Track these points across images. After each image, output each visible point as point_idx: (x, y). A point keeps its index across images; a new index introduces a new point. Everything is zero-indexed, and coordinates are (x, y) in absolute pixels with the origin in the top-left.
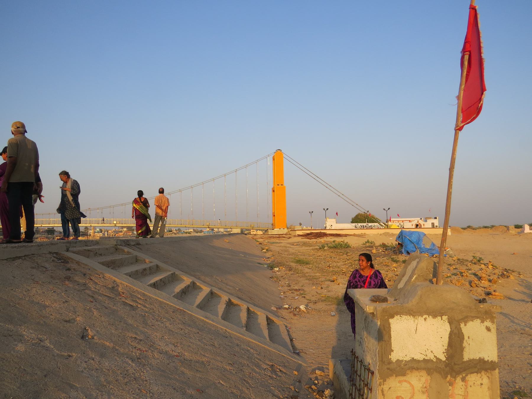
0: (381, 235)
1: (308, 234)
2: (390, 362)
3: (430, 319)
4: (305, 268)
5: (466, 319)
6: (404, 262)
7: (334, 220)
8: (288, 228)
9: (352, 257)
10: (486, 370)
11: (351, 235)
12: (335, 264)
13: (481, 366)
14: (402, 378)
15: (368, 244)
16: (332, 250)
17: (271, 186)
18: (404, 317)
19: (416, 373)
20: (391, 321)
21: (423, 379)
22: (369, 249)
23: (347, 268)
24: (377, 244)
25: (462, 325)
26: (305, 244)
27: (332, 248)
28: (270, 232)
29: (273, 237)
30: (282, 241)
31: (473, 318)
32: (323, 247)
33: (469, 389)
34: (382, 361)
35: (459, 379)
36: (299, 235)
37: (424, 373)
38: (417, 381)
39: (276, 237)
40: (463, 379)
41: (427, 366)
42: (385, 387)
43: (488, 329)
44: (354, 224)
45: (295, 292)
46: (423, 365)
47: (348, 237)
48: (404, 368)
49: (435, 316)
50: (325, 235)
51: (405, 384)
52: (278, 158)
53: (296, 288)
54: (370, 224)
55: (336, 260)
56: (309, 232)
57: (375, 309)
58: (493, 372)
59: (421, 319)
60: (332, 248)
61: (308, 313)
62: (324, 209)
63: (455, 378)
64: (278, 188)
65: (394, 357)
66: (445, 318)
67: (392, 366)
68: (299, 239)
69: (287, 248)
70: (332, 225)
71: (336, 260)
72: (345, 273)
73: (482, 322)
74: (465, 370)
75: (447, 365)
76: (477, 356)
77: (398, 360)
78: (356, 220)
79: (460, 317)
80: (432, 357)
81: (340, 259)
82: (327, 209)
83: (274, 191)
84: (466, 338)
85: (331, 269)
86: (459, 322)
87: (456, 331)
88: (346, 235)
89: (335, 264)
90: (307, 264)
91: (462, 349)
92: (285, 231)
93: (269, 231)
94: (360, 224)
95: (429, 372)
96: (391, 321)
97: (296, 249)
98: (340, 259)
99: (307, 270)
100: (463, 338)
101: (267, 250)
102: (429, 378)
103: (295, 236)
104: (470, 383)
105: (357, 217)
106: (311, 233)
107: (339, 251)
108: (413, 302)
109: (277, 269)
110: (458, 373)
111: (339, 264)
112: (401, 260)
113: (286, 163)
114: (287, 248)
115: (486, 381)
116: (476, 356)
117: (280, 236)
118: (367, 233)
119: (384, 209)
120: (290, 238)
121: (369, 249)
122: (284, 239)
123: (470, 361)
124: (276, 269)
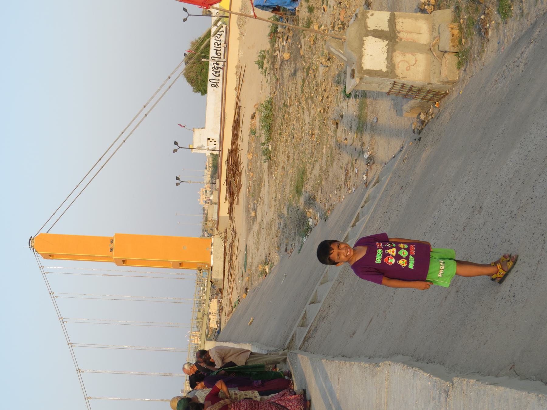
0: (242, 34)
1: (230, 190)
2: (387, 72)
3: (365, 47)
4: (313, 176)
5: (366, 27)
6: (311, 10)
7: (197, 132)
8: (211, 236)
9: (296, 95)
10: (394, 19)
11: (238, 97)
12: (307, 127)
13: (392, 22)
14: (396, 67)
15: (266, 65)
16: (276, 136)
17: (112, 266)
18: (363, 61)
19: (394, 58)
20: (364, 69)
21: (398, 55)
22: (277, 66)
23: (315, 105)
24: (267, 46)
25: (369, 29)
26: (255, 195)
27: (270, 134)
28: (218, 275)
29: (229, 271)
30: (242, 248)
31: (366, 23)
32: (267, 152)
33: (404, 30)
34: (386, 76)
35: (399, 35)
36: (230, 211)
37: (394, 54)
38: (398, 58)
39: (231, 263)
40: (399, 32)
41: (391, 51)
42: (401, 76)
43: (372, 15)
44: (210, 89)
45: (349, 176)
46: (390, 54)
47: (242, 104)
48: (391, 65)
49: (363, 44)
50: (233, 153)
51: (399, 65)
52: (48, 247)
53: (343, 177)
54: (212, 53)
55: (298, 125)
56: (224, 188)
57: (358, 77)
58: (396, 15)
59: (365, 52)
60: (270, 134)
61: (373, 149)
62: (175, 151)
63: (398, 37)
64: (116, 251)
65: (384, 69)
66: (364, 38)
67: (390, 71)
68: (240, 209)
69: (264, 226)
70: (208, 136)
71: (298, 125)
72: (324, 109)
73: (368, 17)
74: (394, 31)
75: (390, 41)
76: (387, 23)
77: (387, 67)
78: (199, 83)
79: (364, 30)
80: (386, 48)
81: (297, 119)
82: (176, 143)
83: (124, 261)
84: (376, 28)
85: (316, 132)
86: (367, 31)
87: (372, 33)
88: (238, 108)
89: (307, 127)
90: (304, 173)
91: (382, 31)
92: (217, 241)
93: (214, 277)
94: (210, 76)
95: (394, 51)
96: (364, 69)
97: (266, 208)
98: (297, 119)
99: (316, 171)
100: (376, 30)
101: (266, 263)
102: (397, 51)
103: (231, 220)
104: (401, 29)
105: (190, 81)
106: (229, 184)
107: (278, 121)
108: (355, 56)
109: (311, 220)
110: (395, 35)
111: (307, 120)
112: (308, 14)
113: (61, 229)
114: (264, 226)
115: (400, 20)
116: (387, 23)
117: (229, 254)
118: (236, 63)
119: (185, 20)
120: (234, 231)
121: (277, 66)
122: (235, 244)
123: (389, 27)
124: (310, 223)
